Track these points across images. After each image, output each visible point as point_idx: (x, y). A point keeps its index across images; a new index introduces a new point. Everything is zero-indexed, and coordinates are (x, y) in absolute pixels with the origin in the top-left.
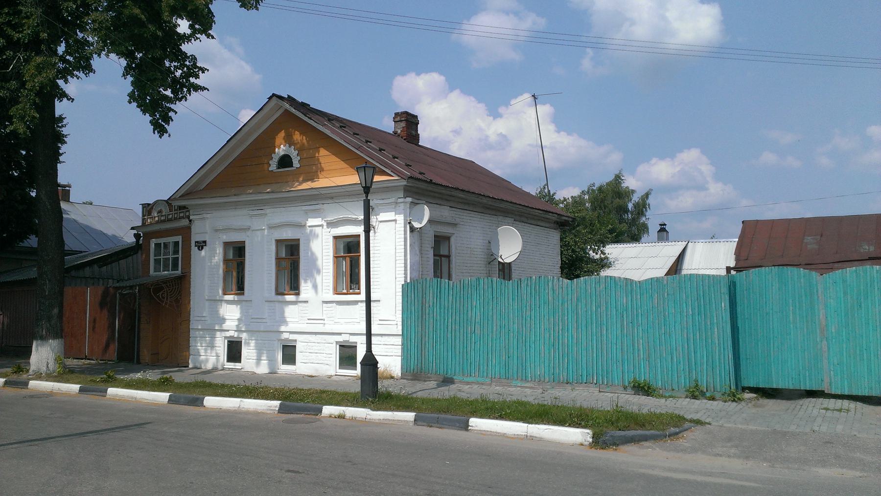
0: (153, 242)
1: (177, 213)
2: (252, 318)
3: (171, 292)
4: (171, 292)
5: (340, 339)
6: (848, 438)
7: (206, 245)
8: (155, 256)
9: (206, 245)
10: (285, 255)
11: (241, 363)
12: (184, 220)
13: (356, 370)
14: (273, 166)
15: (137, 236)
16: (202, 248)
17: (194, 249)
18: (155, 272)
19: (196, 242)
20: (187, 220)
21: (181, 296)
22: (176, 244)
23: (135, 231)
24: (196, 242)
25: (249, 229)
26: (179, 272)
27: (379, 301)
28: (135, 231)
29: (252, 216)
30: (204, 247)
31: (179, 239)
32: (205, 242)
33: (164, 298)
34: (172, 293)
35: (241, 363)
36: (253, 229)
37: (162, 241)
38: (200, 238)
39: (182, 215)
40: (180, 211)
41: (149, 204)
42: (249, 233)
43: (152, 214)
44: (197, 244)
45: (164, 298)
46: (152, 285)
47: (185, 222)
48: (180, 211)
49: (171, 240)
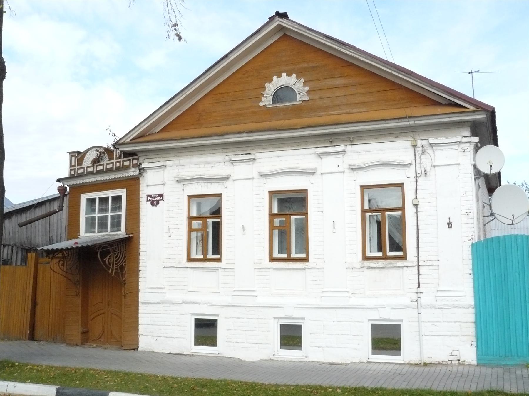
0: (84, 198)
1: (120, 162)
2: (234, 291)
3: (116, 257)
4: (116, 257)
5: (281, 313)
6: (222, 386)
7: (163, 200)
8: (86, 214)
9: (163, 200)
10: (278, 212)
11: (195, 345)
12: (133, 170)
13: (400, 355)
14: (267, 101)
15: (62, 190)
16: (158, 203)
17: (145, 207)
18: (86, 232)
19: (148, 196)
20: (137, 169)
21: (125, 262)
22: (117, 199)
23: (60, 184)
24: (148, 196)
25: (228, 178)
26: (122, 233)
27: (323, 268)
28: (60, 184)
29: (233, 162)
30: (160, 202)
31: (122, 193)
32: (161, 196)
33: (110, 264)
34: (118, 258)
35: (195, 345)
36: (235, 178)
37: (97, 195)
38: (155, 191)
39: (127, 163)
40: (79, 167)
41: (79, 153)
42: (227, 183)
43: (83, 163)
44: (149, 198)
45: (110, 264)
46: (99, 248)
47: (133, 172)
48: (79, 167)
49: (110, 194)
